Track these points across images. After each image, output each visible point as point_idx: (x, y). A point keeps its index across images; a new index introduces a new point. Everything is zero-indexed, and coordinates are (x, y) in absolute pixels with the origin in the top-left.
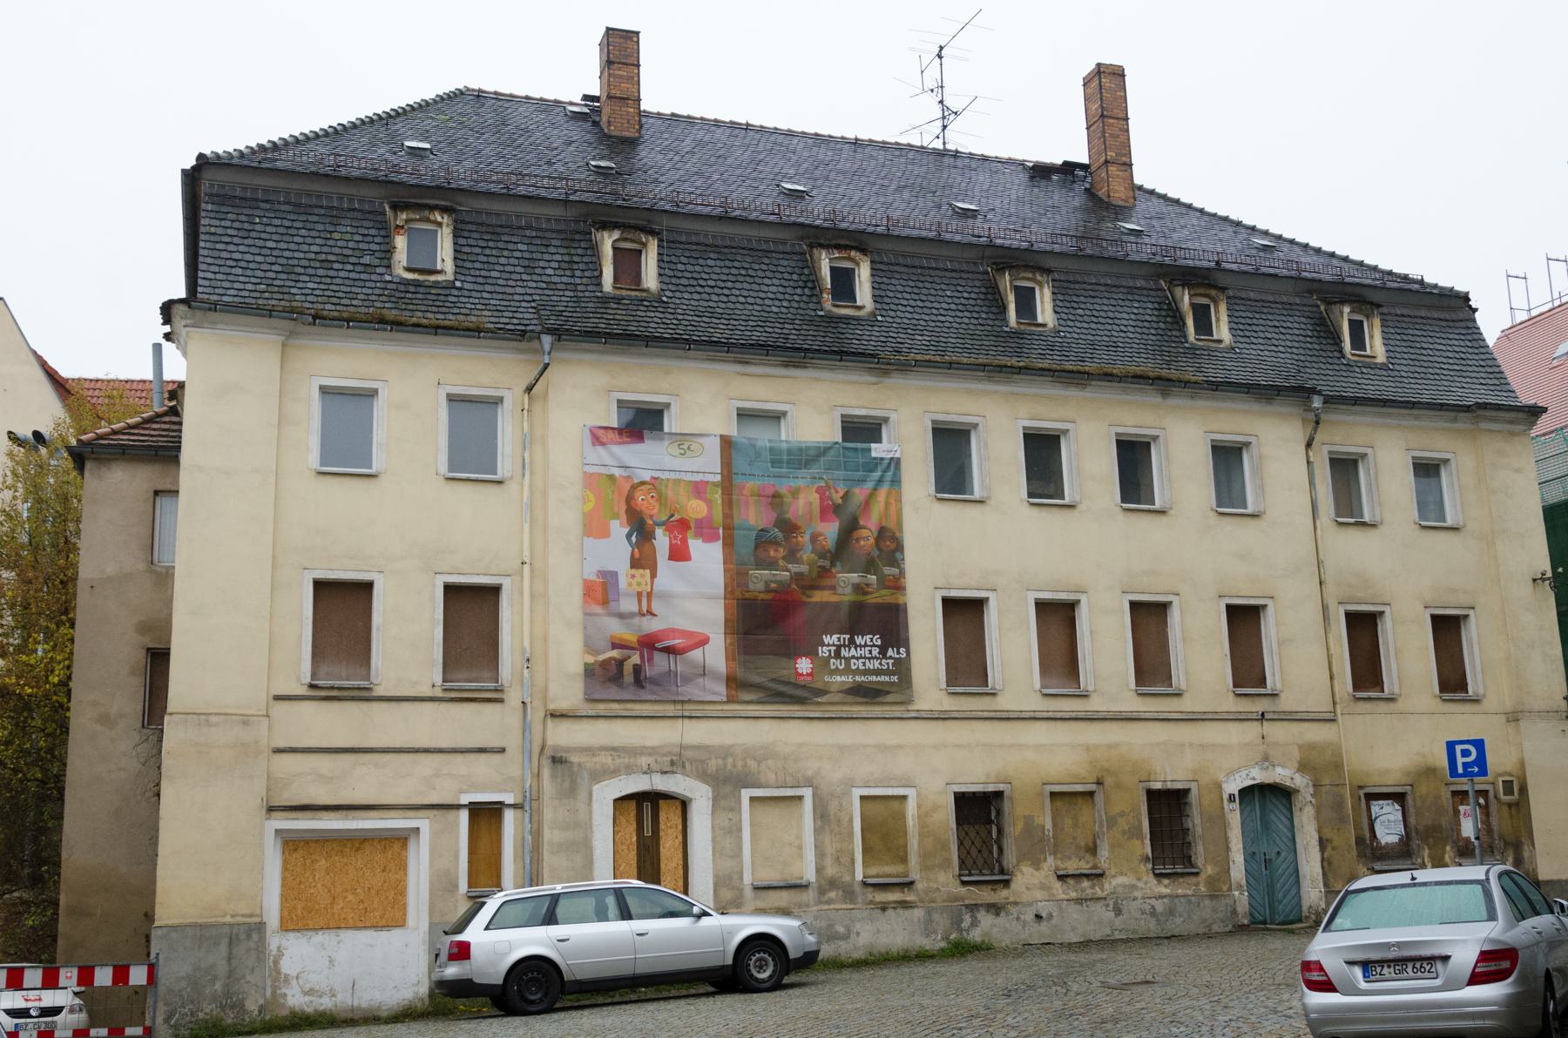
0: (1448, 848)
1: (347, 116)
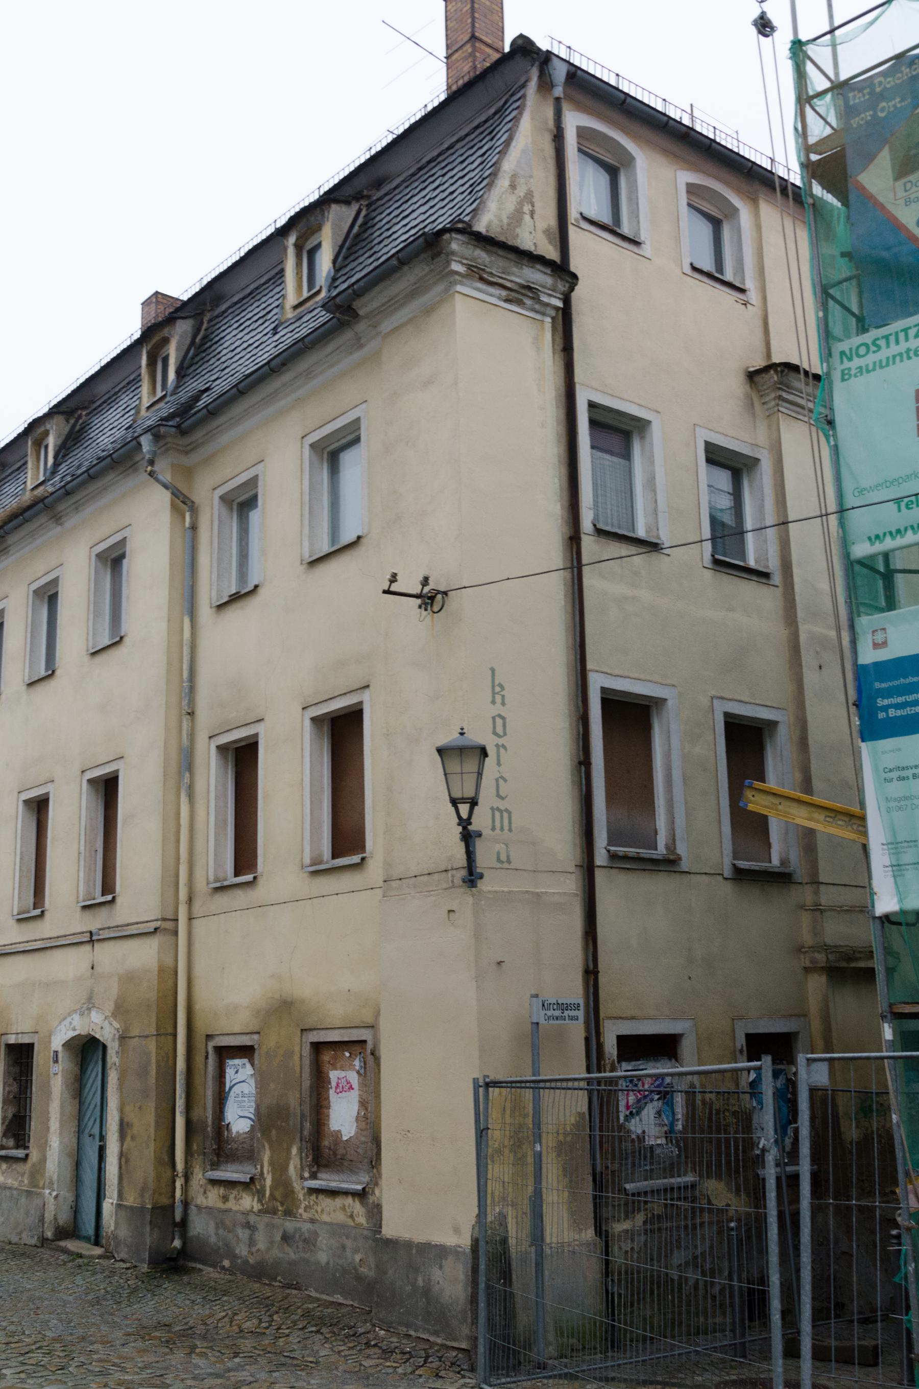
0: (294, 1151)
1: (379, 139)
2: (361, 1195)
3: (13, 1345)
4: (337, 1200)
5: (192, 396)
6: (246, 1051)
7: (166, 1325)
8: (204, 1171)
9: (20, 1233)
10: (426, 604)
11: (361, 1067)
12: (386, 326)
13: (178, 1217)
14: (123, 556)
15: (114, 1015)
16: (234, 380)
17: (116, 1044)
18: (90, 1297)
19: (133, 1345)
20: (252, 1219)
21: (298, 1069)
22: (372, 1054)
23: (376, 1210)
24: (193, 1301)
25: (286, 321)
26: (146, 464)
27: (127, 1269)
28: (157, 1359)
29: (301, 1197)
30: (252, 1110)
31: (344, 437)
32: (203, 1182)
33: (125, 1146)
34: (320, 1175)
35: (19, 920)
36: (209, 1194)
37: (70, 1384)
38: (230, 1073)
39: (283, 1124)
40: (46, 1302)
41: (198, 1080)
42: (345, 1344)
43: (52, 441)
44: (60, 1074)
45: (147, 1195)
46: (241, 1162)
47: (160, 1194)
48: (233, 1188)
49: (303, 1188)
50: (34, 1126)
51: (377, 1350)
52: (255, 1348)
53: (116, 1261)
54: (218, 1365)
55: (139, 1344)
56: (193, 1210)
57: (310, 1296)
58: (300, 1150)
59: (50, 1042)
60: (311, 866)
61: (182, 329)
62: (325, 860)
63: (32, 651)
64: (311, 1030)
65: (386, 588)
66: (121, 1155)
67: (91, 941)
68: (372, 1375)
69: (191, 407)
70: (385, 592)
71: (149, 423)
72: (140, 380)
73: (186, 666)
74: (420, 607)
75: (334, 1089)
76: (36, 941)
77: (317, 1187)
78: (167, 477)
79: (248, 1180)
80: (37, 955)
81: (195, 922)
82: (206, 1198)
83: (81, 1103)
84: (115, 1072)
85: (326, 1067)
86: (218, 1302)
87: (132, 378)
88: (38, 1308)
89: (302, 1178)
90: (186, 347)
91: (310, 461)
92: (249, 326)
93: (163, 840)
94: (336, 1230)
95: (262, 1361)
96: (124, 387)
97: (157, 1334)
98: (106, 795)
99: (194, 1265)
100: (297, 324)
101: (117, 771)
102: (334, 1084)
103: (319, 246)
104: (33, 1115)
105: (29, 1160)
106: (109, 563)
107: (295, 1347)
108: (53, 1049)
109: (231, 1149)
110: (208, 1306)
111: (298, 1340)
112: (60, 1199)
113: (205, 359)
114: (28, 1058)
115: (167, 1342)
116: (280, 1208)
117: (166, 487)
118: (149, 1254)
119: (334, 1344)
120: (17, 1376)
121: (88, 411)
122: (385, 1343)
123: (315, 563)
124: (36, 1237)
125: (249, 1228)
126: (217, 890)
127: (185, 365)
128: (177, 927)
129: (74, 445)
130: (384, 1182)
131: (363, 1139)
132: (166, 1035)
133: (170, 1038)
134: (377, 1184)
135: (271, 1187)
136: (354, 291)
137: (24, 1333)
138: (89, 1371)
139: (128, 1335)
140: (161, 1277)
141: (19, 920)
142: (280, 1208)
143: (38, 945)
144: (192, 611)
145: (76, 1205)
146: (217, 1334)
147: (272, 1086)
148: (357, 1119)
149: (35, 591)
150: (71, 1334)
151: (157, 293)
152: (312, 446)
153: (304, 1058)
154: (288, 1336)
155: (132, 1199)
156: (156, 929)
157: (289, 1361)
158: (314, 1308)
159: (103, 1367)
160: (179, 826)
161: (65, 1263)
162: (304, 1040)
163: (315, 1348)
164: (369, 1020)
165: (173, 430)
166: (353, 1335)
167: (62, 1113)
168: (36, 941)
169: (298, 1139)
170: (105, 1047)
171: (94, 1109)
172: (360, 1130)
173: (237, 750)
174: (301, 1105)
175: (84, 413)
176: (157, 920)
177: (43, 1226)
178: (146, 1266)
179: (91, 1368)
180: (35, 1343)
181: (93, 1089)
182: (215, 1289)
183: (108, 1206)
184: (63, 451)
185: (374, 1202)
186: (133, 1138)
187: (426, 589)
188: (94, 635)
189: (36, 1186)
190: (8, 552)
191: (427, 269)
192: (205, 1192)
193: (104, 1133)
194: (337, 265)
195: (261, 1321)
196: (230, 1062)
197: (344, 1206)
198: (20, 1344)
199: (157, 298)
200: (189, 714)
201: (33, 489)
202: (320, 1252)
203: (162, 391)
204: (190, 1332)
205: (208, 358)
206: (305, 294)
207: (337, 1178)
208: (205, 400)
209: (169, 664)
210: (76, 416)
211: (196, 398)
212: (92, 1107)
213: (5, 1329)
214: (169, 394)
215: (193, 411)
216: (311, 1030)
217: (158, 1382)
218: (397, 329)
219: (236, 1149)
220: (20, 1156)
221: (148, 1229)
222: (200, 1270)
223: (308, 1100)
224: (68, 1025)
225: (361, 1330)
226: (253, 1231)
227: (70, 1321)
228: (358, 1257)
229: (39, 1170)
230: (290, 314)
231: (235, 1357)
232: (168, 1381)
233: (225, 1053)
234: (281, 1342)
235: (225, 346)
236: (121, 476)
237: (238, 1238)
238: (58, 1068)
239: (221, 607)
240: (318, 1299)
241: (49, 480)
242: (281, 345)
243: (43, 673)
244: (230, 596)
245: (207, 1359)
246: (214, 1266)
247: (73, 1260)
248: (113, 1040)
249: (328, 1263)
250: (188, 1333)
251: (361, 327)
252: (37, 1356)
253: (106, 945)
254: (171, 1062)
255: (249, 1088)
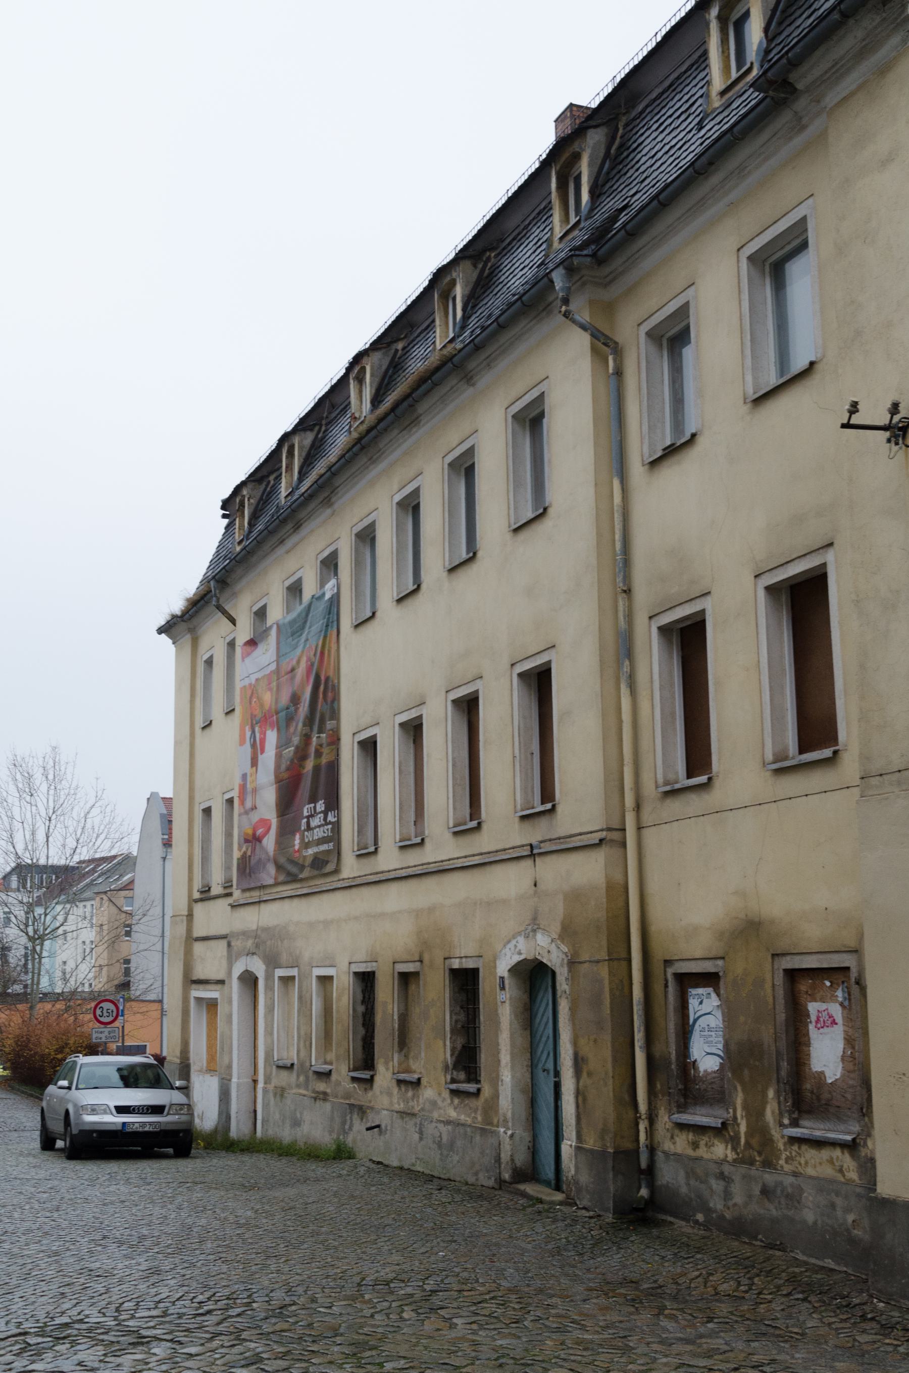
0: (771, 1093)
2: (852, 1147)
3: (465, 1293)
4: (823, 1152)
5: (608, 218)
6: (710, 979)
7: (633, 1282)
8: (671, 1114)
9: (476, 1174)
10: (896, 437)
11: (845, 999)
12: (831, 99)
13: (644, 1164)
14: (542, 415)
15: (561, 937)
16: (653, 191)
17: (565, 970)
18: (550, 1247)
19: (594, 1301)
20: (727, 1169)
21: (770, 1000)
22: (858, 983)
23: (869, 1165)
24: (663, 1258)
25: (712, 112)
26: (559, 302)
27: (591, 1217)
28: (621, 1319)
29: (781, 1146)
30: (721, 1046)
31: (789, 243)
32: (669, 1125)
33: (581, 1084)
34: (802, 1122)
35: (456, 834)
36: (677, 1139)
37: (524, 1339)
38: (693, 1003)
39: (757, 1063)
40: (503, 1249)
41: (658, 1012)
42: (836, 1316)
43: (459, 291)
44: (508, 1002)
45: (608, 1138)
46: (711, 1105)
47: (622, 1137)
48: (704, 1134)
49: (783, 1137)
50: (484, 1058)
51: (874, 1324)
52: (731, 1313)
53: (578, 1208)
54: (688, 1330)
55: (602, 1301)
56: (660, 1156)
57: (797, 1259)
58: (778, 1093)
59: (495, 967)
60: (774, 762)
61: (595, 138)
62: (791, 755)
63: (451, 532)
64: (784, 955)
65: (845, 421)
66: (578, 1093)
67: (532, 855)
68: (868, 1352)
69: (608, 230)
70: (844, 426)
71: (562, 255)
72: (551, 209)
73: (618, 536)
74: (889, 441)
75: (814, 1024)
76: (474, 855)
77: (799, 1135)
78: (585, 316)
79: (720, 1126)
80: (476, 872)
81: (645, 832)
82: (674, 1143)
83: (532, 1035)
84: (566, 1001)
85: (803, 998)
86: (690, 1260)
87: (542, 206)
88: (494, 1255)
89: (781, 1125)
90: (599, 161)
91: (749, 275)
92: (670, 124)
93: (604, 739)
94: (823, 1185)
95: (740, 1329)
96: (534, 219)
97: (622, 1291)
98: (539, 690)
99: (664, 1217)
100: (725, 113)
101: (549, 662)
102: (813, 1018)
103: (747, 14)
104: (483, 1046)
105: (482, 1095)
106: (528, 424)
107: (778, 1315)
108: (499, 974)
109: (699, 1089)
110: (680, 1264)
111: (782, 1307)
112: (517, 1138)
113: (622, 172)
114: (474, 985)
115: (633, 1300)
116: (758, 1158)
117: (583, 327)
118: (614, 1202)
119: (824, 1314)
120: (468, 1327)
121: (497, 252)
122: (884, 1317)
123: (760, 400)
124: (493, 1179)
125: (724, 1179)
126: (667, 794)
127: (600, 182)
128: (625, 838)
129: (484, 293)
130: (877, 1131)
131: (851, 1082)
132: (619, 960)
133: (624, 964)
134: (869, 1135)
135: (746, 1133)
136: (788, 59)
137: (477, 1281)
138: (546, 1326)
139: (590, 1290)
140: (627, 1228)
141: (456, 834)
142: (758, 1158)
143: (477, 860)
144: (621, 469)
145: (534, 1146)
146: (689, 1295)
147: (742, 1019)
148: (843, 1058)
149: (450, 465)
150: (528, 1285)
151: (571, 105)
152: (750, 258)
153: (777, 988)
154: (770, 1302)
155: (592, 1142)
156: (601, 840)
157: (772, 1331)
158: (801, 1272)
159: (560, 1323)
160: (620, 721)
161: (524, 1208)
162: (776, 967)
163: (801, 1318)
164: (852, 943)
165: (589, 259)
166: (847, 1306)
167: (513, 1045)
168: (474, 855)
169: (774, 1081)
170: (554, 973)
171: (547, 1041)
172: (847, 1071)
173: (682, 630)
174: (776, 1041)
175: (493, 255)
176: (602, 830)
177: (500, 1167)
178: (611, 1216)
179: (547, 1323)
180: (489, 1292)
181: (545, 1020)
182: (688, 1246)
183: (567, 1148)
184: (472, 301)
185: (866, 1155)
186: (590, 1074)
187: (896, 418)
188: (516, 508)
189: (491, 1124)
190: (419, 422)
191: (878, 19)
192: (672, 1137)
193: (559, 1069)
194: (770, 34)
195: (739, 1284)
196: (693, 991)
197: (832, 1158)
198: (472, 1293)
199: (571, 111)
200: (625, 591)
201: (441, 349)
202: (806, 1210)
203: (576, 217)
204: (659, 1291)
205: (625, 170)
206: (734, 75)
207: (822, 1127)
208: (623, 218)
209: (599, 535)
210: (484, 259)
211: (614, 219)
212: (544, 1039)
213: (457, 1276)
214: (583, 218)
215: (609, 236)
216: (784, 955)
217: (620, 1344)
218: (845, 99)
219: (705, 1090)
220: (472, 1090)
221: (611, 1175)
222: (671, 1223)
223: (784, 1036)
224: (513, 948)
225: (856, 1301)
226: (728, 1182)
227: (528, 1272)
228: (850, 1218)
229: (491, 1107)
230: (717, 103)
231: (708, 1322)
232: (631, 1344)
233: (686, 981)
234: (762, 1308)
235: (644, 152)
236: (534, 321)
237: (712, 1190)
238: (505, 996)
239: (654, 464)
240: (806, 1263)
241: (459, 336)
242: (708, 141)
243: (464, 556)
244: (664, 450)
245: (677, 1321)
246: (686, 1219)
247: (533, 1205)
248: (562, 965)
249: (815, 1223)
250: (656, 1292)
251: (801, 104)
252: (490, 1307)
253: (548, 859)
254: (626, 990)
255: (715, 1021)
